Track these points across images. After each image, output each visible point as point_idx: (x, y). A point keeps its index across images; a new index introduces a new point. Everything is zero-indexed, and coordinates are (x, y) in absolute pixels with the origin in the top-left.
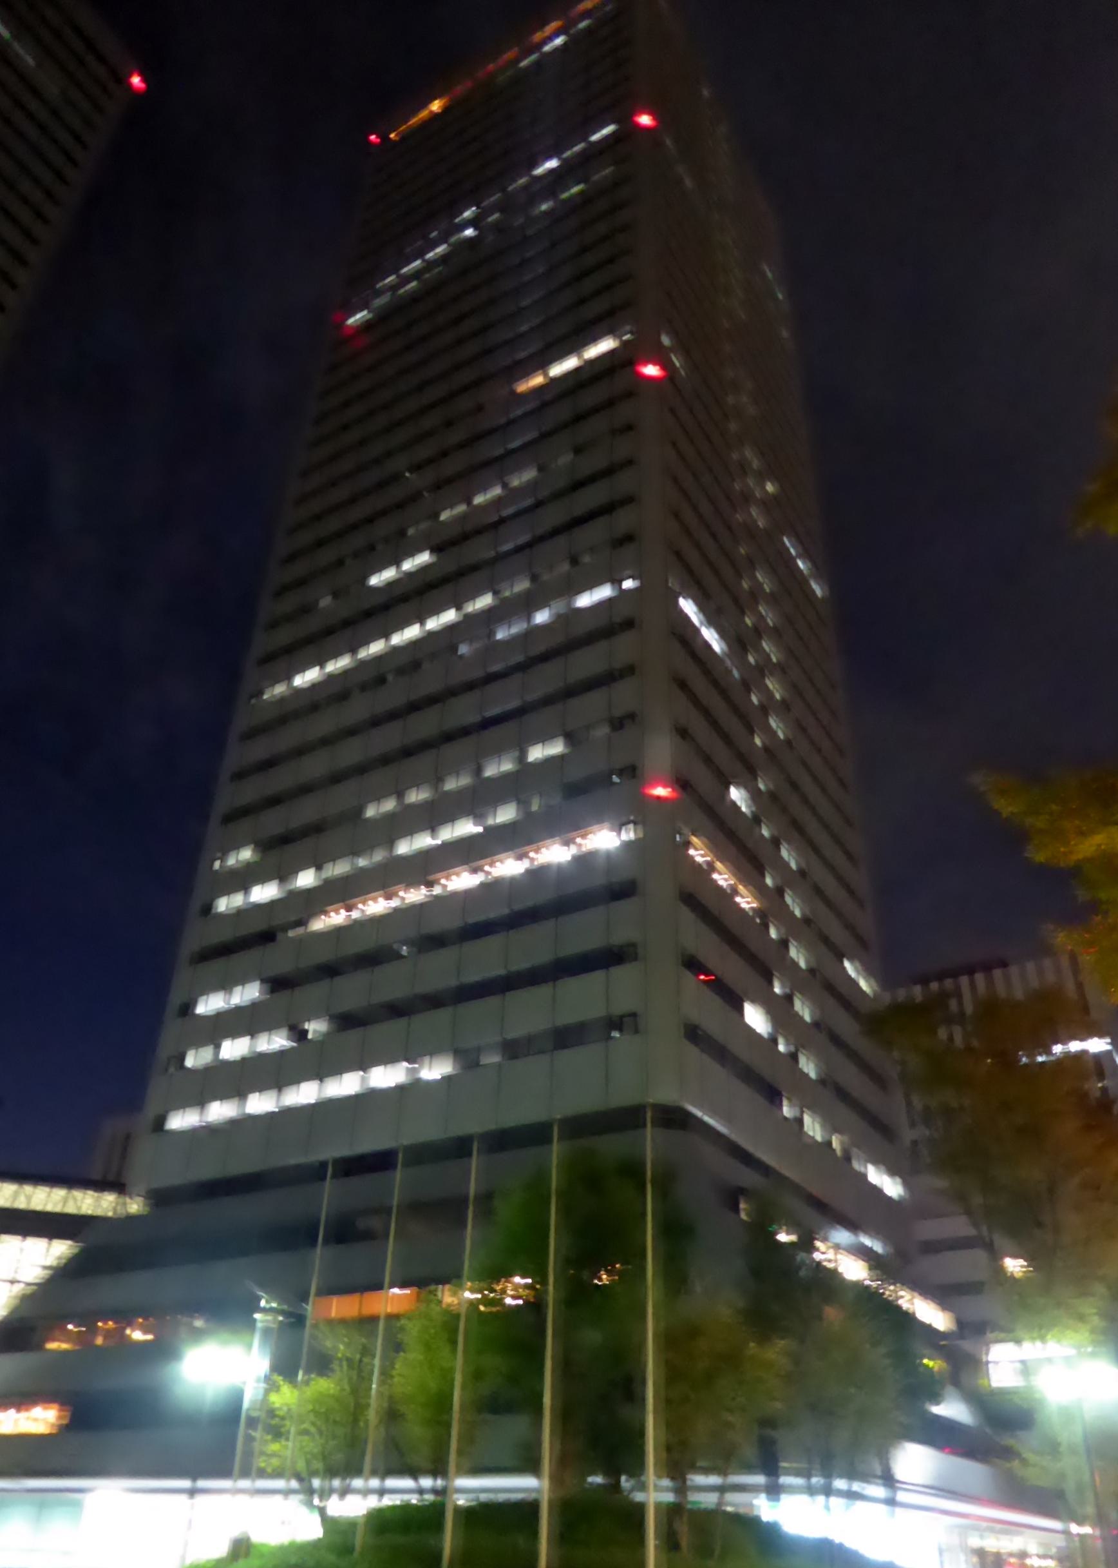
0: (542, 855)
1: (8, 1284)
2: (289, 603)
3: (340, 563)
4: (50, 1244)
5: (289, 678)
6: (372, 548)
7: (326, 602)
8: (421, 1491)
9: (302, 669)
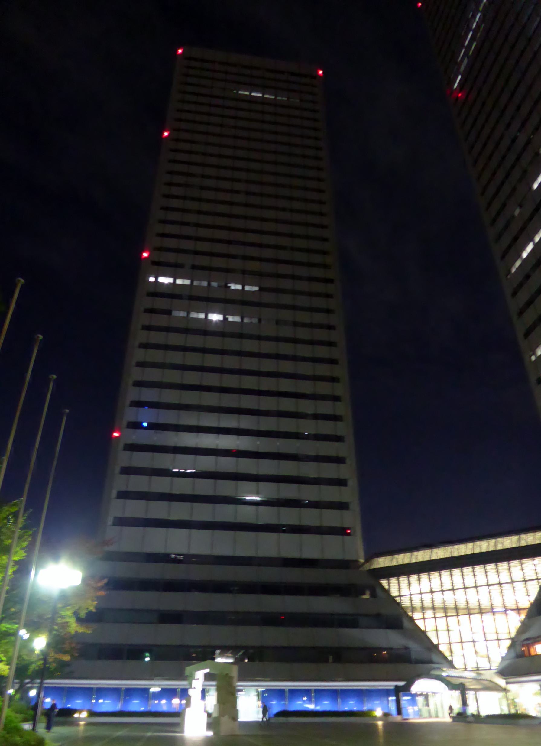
0: (525, 570)
1: (462, 655)
2: (501, 223)
3: (514, 189)
4: (403, 708)
5: (519, 256)
6: (525, 172)
7: (517, 212)
8: (204, 693)
9: (524, 248)
